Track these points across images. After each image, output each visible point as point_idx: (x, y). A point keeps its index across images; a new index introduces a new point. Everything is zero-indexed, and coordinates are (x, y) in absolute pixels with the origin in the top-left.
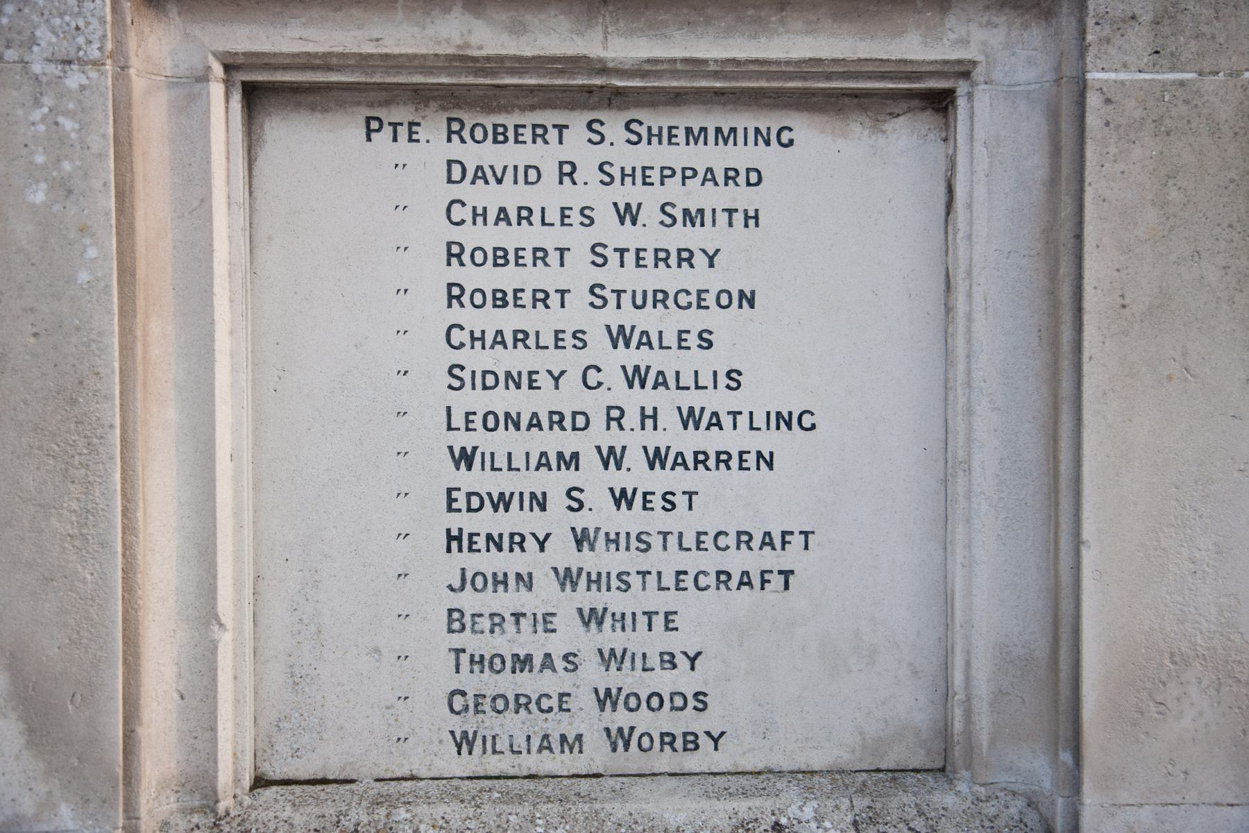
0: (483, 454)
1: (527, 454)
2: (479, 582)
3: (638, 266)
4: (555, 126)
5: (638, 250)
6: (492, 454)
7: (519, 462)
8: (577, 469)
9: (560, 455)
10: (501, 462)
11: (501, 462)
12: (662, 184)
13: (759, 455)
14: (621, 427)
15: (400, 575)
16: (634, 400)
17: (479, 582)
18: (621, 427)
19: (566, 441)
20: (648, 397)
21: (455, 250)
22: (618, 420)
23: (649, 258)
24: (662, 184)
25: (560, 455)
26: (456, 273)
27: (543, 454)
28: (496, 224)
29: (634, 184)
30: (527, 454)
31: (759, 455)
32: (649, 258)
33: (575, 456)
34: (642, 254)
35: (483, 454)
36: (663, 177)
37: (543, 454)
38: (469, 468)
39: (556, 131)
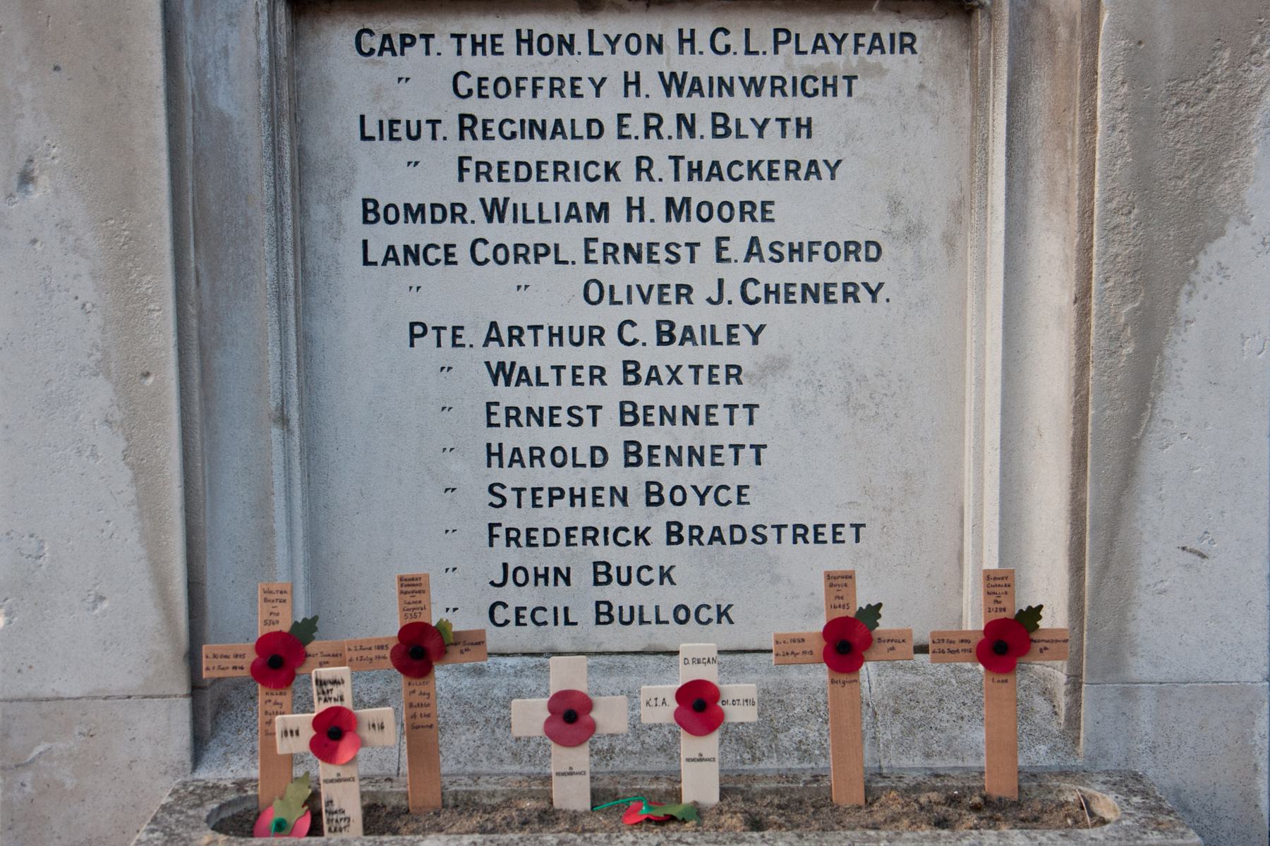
0: (515, 206)
1: (557, 204)
2: (521, 577)
3: (574, 383)
4: (530, 327)
5: (574, 368)
6: (524, 205)
7: (549, 213)
8: (607, 220)
9: (590, 206)
10: (533, 213)
11: (533, 213)
12: (551, 505)
13: (662, 409)
14: (659, 136)
15: (442, 368)
16: (670, 107)
17: (521, 577)
18: (659, 136)
19: (597, 193)
20: (687, 105)
21: (468, 122)
22: (657, 128)
23: (585, 375)
24: (551, 505)
25: (590, 206)
26: (498, 474)
27: (573, 205)
28: (510, 466)
29: (536, 569)
30: (557, 204)
31: (662, 409)
32: (585, 375)
33: (605, 206)
34: (578, 372)
35: (515, 206)
36: (552, 498)
37: (573, 205)
38: (501, 220)
39: (532, 332)
